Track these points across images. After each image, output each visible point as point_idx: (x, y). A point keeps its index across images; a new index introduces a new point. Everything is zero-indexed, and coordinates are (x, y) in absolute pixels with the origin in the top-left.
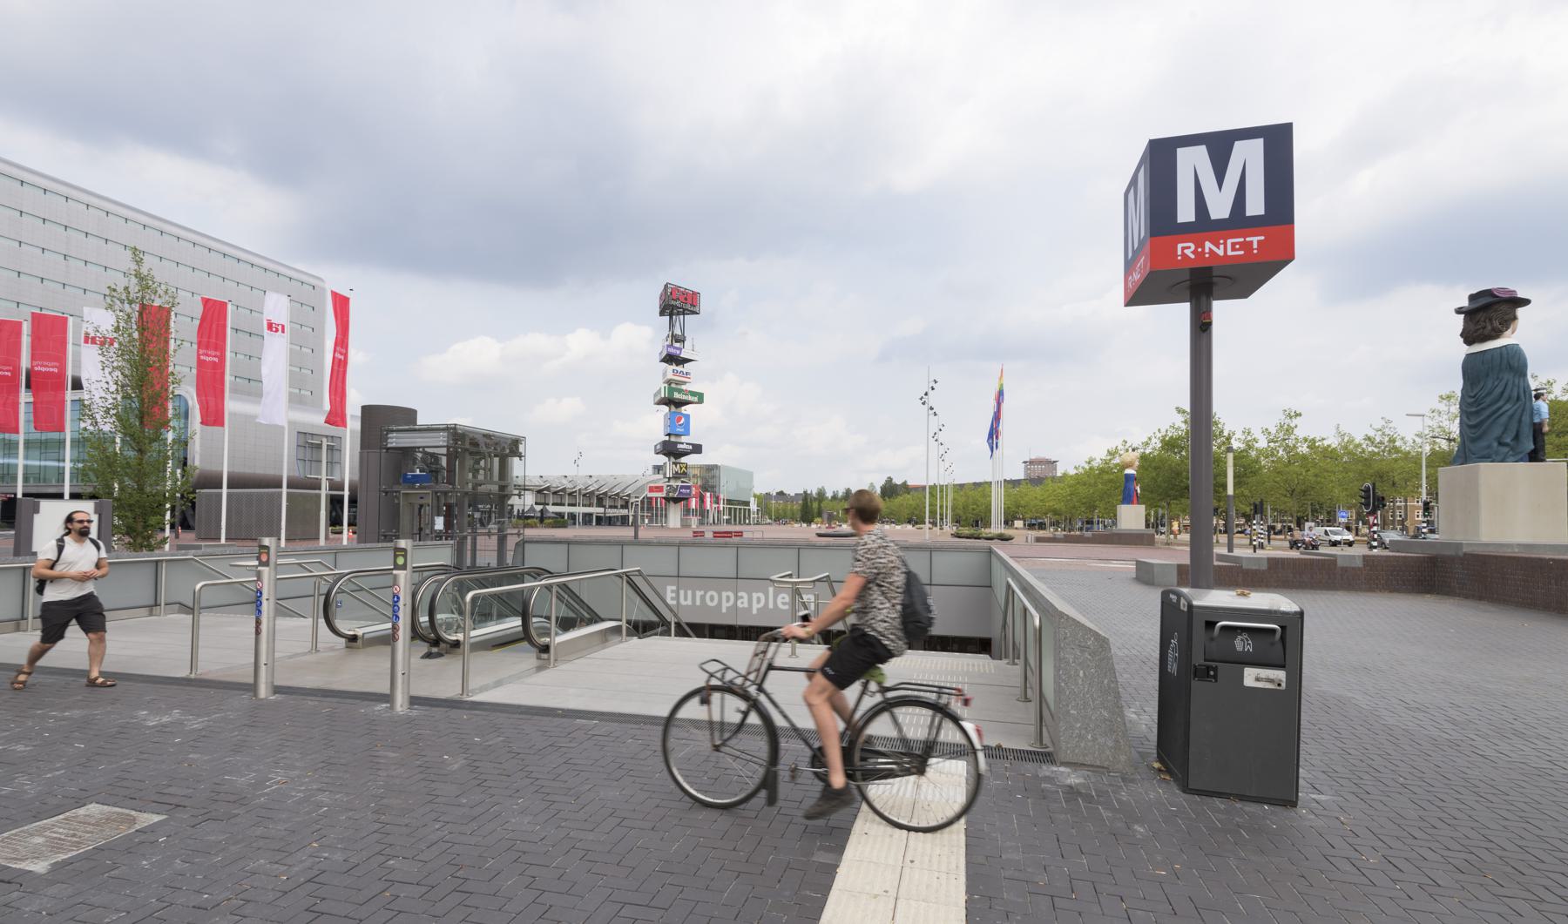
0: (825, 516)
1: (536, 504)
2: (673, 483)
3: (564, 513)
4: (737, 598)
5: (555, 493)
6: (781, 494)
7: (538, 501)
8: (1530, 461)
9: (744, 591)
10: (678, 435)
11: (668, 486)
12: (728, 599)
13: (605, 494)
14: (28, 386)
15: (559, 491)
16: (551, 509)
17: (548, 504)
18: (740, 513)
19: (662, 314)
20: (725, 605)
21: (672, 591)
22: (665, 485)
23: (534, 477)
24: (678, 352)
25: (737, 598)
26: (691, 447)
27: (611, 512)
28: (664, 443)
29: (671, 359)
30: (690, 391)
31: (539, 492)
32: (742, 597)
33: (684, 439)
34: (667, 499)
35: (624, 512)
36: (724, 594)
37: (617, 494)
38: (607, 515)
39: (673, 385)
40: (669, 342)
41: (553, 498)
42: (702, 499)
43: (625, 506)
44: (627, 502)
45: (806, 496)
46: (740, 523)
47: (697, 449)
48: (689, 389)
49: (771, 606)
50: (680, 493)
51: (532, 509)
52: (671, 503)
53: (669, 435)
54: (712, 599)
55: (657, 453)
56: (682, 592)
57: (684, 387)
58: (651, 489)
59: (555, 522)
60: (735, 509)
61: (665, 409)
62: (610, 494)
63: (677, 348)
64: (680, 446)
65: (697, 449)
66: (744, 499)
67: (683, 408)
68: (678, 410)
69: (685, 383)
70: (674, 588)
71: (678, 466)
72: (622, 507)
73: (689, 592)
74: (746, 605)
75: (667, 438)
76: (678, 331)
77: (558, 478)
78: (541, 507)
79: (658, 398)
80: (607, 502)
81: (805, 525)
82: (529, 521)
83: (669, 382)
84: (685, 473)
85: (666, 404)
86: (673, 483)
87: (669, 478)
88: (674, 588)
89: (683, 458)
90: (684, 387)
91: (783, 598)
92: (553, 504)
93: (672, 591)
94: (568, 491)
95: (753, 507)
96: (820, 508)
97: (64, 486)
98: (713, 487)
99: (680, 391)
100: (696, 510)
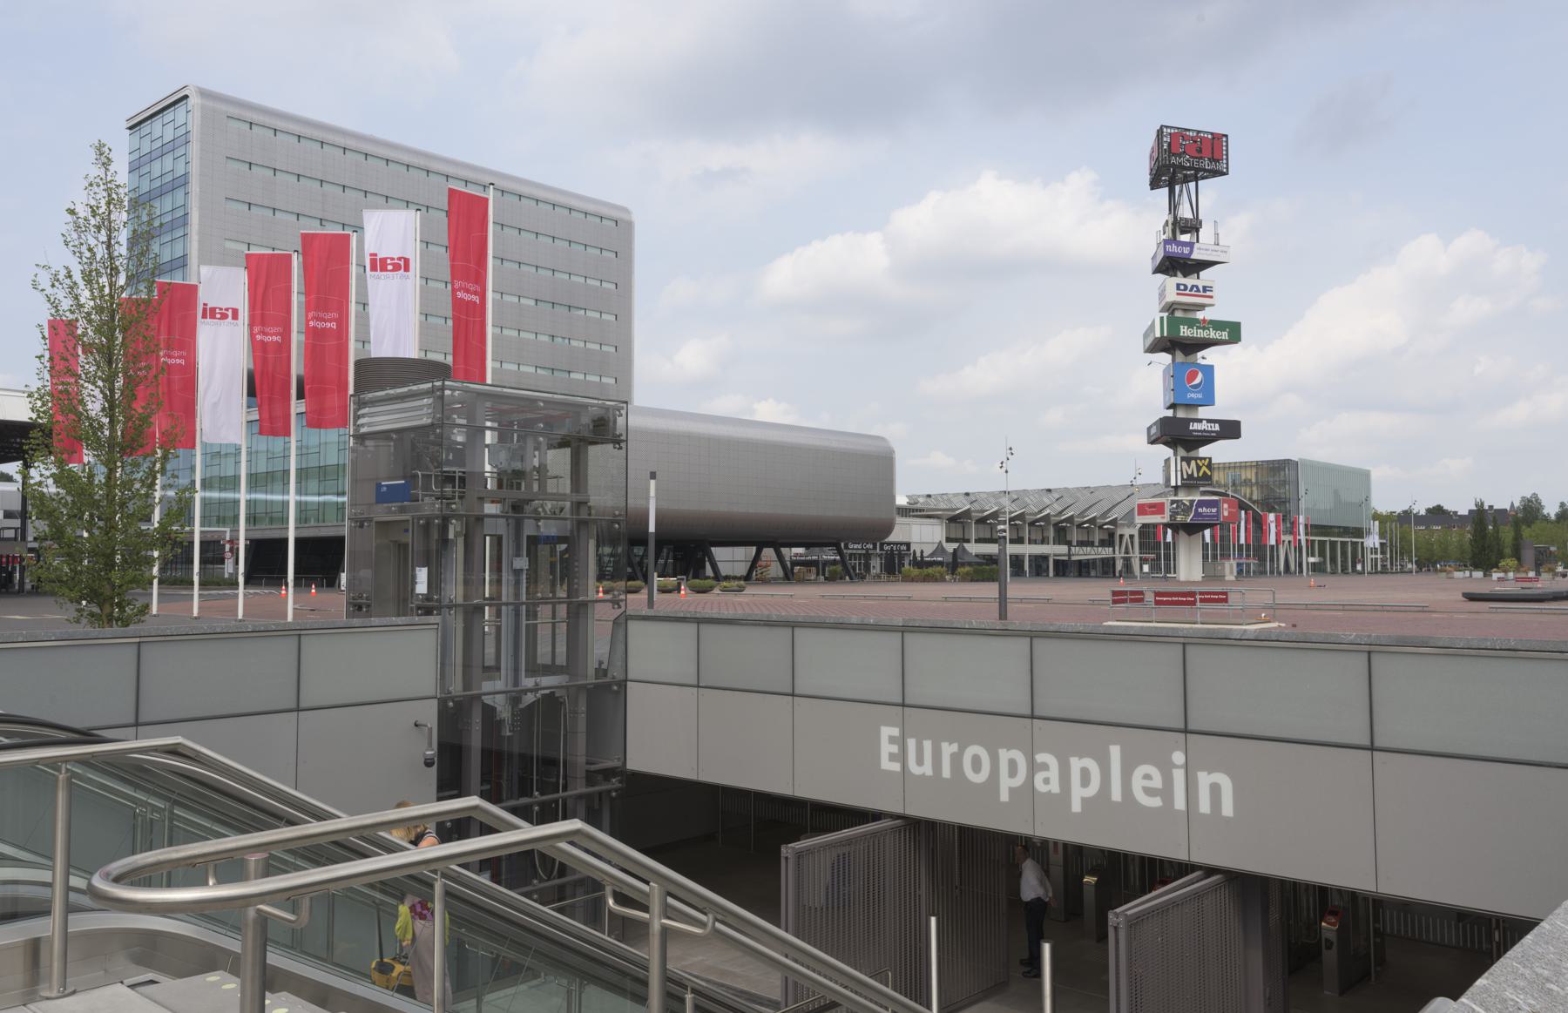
0: (1528, 555)
1: (949, 540)
2: (1184, 497)
3: (1023, 556)
4: (1033, 768)
5: (1032, 524)
6: (1437, 513)
7: (953, 536)
8: (483, 750)
9: (1051, 751)
10: (1193, 406)
11: (1173, 502)
12: (1013, 765)
13: (1070, 520)
14: (300, 396)
15: (1038, 520)
16: (973, 548)
17: (968, 541)
18: (1344, 553)
19: (1154, 184)
20: (1006, 783)
21: (892, 740)
22: (1166, 500)
23: (956, 495)
24: (1186, 250)
25: (1033, 768)
26: (1217, 428)
27: (1081, 554)
28: (1164, 422)
29: (1173, 264)
30: (1211, 322)
31: (953, 520)
32: (1045, 767)
33: (1203, 412)
34: (1176, 527)
35: (1106, 552)
36: (1004, 755)
37: (1092, 521)
38: (1074, 558)
39: (1179, 314)
40: (1169, 234)
41: (977, 530)
42: (1259, 524)
43: (1109, 541)
44: (1112, 535)
45: (1481, 516)
46: (1344, 570)
47: (1230, 430)
48: (1208, 318)
49: (1116, 795)
50: (1197, 514)
51: (940, 549)
52: (1182, 533)
53: (1173, 406)
54: (976, 764)
55: (1152, 442)
56: (911, 743)
57: (1200, 315)
58: (1143, 510)
59: (976, 571)
60: (1333, 544)
61: (1165, 358)
62: (1100, 521)
63: (1184, 244)
64: (1195, 426)
65: (1230, 430)
66: (1351, 523)
67: (1200, 354)
68: (1190, 358)
69: (1202, 307)
70: (895, 732)
71: (1193, 463)
72: (1103, 543)
73: (928, 745)
74: (1055, 787)
75: (1170, 413)
76: (1185, 212)
77: (993, 495)
78: (955, 545)
79: (1150, 340)
80: (1075, 536)
81: (1479, 574)
82: (930, 570)
83: (1171, 308)
84: (1207, 478)
85: (1166, 350)
86: (1184, 497)
87: (1176, 488)
88: (895, 732)
89: (1201, 449)
90: (1200, 315)
91: (1147, 777)
92: (977, 541)
93: (892, 740)
94: (1030, 518)
95: (1373, 541)
96: (1518, 537)
97: (288, 528)
98: (1284, 502)
99: (1192, 323)
100: (1248, 546)
